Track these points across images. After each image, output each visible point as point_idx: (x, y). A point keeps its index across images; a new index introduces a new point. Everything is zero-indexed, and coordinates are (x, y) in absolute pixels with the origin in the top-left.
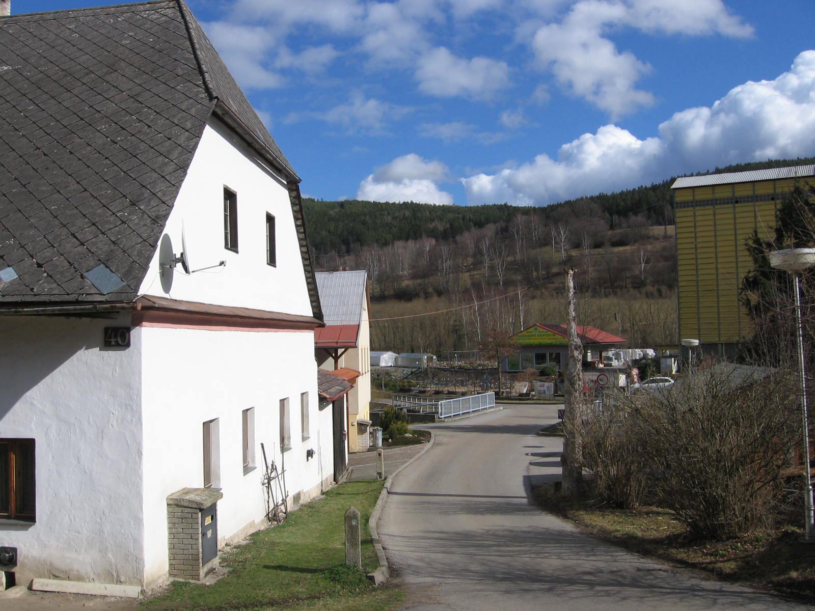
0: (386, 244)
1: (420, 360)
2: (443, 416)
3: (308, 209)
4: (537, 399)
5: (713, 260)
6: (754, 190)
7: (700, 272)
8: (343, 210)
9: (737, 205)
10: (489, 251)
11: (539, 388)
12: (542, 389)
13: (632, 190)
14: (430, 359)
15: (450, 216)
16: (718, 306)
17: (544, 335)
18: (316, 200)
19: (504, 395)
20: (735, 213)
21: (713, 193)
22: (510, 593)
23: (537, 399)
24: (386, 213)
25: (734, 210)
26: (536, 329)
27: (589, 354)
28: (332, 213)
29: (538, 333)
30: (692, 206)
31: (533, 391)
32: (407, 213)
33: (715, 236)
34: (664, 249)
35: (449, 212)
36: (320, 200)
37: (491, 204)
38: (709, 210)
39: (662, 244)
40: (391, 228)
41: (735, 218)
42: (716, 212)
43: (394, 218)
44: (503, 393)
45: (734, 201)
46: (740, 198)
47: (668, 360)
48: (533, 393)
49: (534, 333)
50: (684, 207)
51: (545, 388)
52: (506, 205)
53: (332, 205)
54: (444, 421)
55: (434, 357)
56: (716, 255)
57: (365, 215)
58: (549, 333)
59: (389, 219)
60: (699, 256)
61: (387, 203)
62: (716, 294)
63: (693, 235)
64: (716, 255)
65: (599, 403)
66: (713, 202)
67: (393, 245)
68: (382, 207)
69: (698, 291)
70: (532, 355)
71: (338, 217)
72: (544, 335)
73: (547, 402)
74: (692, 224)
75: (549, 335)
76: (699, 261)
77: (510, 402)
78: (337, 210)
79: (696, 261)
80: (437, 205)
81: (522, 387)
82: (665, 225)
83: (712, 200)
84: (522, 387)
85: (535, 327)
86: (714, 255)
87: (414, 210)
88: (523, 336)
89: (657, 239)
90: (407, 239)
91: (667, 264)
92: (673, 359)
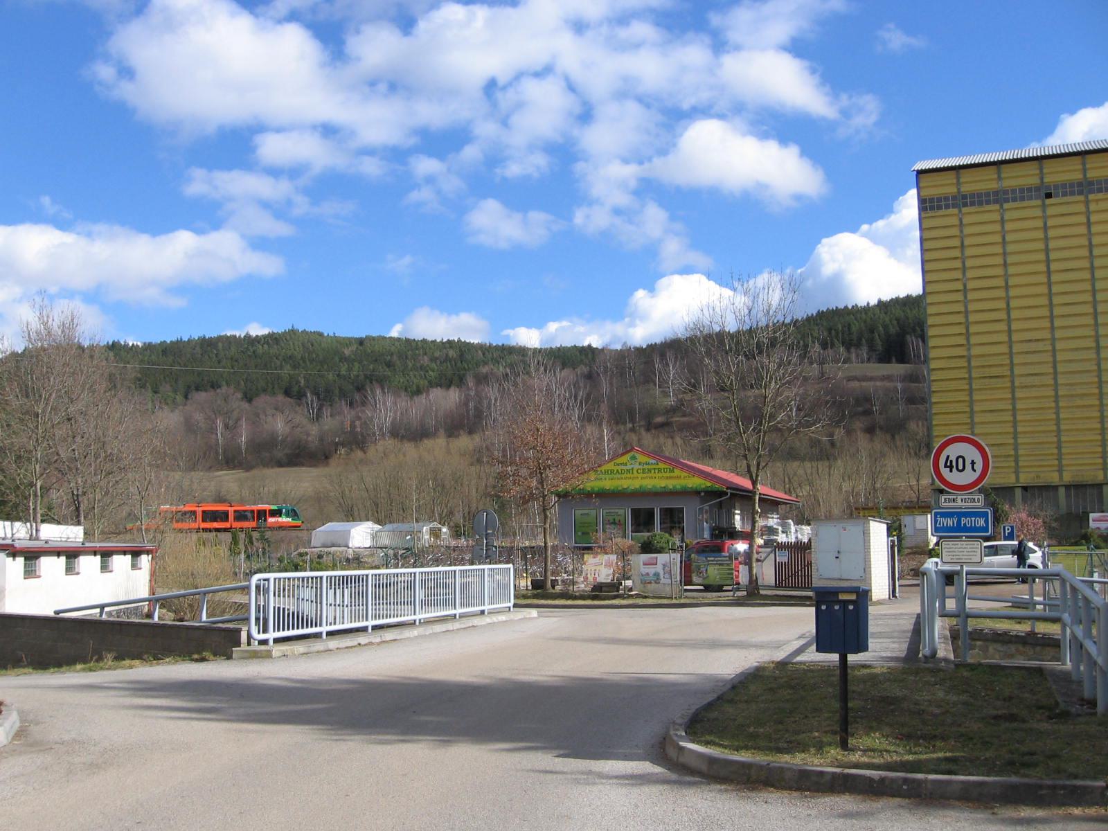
0: (418, 392)
1: (416, 534)
2: (271, 635)
3: (312, 345)
4: (638, 596)
5: (1003, 315)
6: (1085, 171)
7: (973, 340)
8: (361, 348)
9: (1048, 201)
11: (644, 570)
12: (651, 570)
14: (435, 533)
16: (1014, 410)
17: (650, 471)
18: (326, 334)
20: (1045, 218)
21: (1000, 178)
23: (638, 596)
24: (421, 353)
25: (1044, 211)
26: (634, 458)
27: (737, 518)
28: (347, 352)
29: (637, 466)
30: (954, 206)
31: (628, 579)
32: (451, 353)
33: (1005, 265)
36: (331, 334)
37: (569, 346)
38: (991, 213)
40: (427, 372)
41: (1045, 228)
42: (1006, 217)
43: (434, 359)
44: (554, 583)
45: (1043, 193)
46: (1056, 187)
48: (629, 583)
49: (629, 467)
50: (940, 208)
51: (659, 568)
52: (589, 346)
53: (349, 342)
54: (268, 655)
55: (444, 530)
56: (1008, 305)
57: (392, 355)
58: (661, 466)
59: (425, 360)
60: (971, 307)
61: (424, 341)
62: (1009, 385)
63: (958, 264)
64: (1008, 305)
66: (999, 197)
67: (428, 395)
68: (417, 345)
69: (970, 378)
71: (353, 356)
72: (650, 471)
74: (956, 242)
75: (659, 470)
76: (972, 318)
77: (570, 602)
78: (354, 347)
79: (967, 317)
80: (494, 345)
81: (599, 568)
83: (996, 193)
84: (599, 568)
86: (1002, 305)
87: (461, 350)
88: (606, 472)
90: (448, 387)
92: (929, 516)
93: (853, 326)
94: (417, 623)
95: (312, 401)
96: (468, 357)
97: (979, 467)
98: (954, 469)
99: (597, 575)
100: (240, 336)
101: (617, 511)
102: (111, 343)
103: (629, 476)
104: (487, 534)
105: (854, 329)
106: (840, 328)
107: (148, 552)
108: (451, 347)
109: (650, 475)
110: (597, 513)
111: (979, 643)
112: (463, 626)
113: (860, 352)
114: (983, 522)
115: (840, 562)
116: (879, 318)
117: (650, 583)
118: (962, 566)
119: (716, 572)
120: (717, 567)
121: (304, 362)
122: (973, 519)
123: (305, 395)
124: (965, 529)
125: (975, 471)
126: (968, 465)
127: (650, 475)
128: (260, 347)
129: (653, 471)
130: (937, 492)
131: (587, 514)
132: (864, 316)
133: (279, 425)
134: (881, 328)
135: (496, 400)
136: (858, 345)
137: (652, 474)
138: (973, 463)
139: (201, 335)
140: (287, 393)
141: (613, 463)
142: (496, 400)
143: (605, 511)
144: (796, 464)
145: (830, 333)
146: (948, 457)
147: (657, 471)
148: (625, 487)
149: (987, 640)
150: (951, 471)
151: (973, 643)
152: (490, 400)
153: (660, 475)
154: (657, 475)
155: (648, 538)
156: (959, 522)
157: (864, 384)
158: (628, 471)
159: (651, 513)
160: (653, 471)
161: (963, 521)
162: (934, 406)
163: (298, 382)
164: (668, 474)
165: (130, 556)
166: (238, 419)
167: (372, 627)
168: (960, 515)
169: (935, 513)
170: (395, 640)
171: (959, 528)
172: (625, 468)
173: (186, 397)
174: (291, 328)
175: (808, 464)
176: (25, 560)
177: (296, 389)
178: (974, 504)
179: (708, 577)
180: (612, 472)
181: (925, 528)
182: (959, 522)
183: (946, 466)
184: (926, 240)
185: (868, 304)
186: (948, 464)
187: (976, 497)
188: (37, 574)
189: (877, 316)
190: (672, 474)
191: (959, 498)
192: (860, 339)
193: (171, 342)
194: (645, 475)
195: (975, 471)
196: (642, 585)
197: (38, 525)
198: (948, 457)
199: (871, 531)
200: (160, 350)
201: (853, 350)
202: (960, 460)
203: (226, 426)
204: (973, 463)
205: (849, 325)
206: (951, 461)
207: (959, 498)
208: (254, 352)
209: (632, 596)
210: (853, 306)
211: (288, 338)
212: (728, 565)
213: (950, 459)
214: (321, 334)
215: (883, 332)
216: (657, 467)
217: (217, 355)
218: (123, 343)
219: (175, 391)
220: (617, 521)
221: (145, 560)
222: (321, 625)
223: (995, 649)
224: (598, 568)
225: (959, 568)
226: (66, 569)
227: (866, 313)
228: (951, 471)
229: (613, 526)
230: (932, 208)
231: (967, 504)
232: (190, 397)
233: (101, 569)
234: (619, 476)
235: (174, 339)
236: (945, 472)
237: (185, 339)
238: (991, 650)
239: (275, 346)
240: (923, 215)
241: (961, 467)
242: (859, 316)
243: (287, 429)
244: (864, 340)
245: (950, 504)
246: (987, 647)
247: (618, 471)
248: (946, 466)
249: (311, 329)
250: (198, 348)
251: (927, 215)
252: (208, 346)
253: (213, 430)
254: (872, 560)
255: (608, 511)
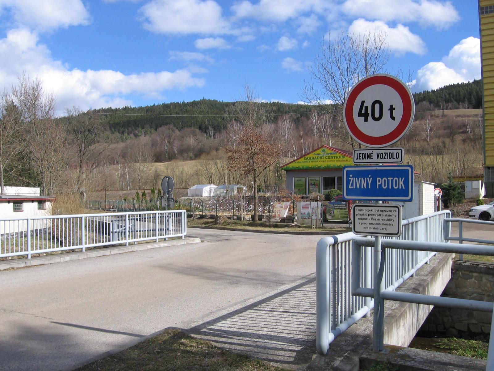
4: (296, 226)
10: (317, 122)
11: (303, 211)
13: (419, 93)
15: (302, 110)
17: (332, 157)
19: (264, 219)
22: (458, 115)
26: (324, 151)
29: (325, 156)
32: (274, 108)
34: (443, 123)
35: (301, 108)
36: (221, 101)
39: (441, 120)
47: (475, 183)
49: (321, 155)
55: (244, 188)
58: (338, 155)
65: (358, 246)
70: (320, 179)
72: (332, 157)
73: (306, 230)
75: (337, 157)
82: (443, 109)
84: (282, 210)
85: (323, 149)
88: (310, 158)
89: (438, 117)
91: (444, 131)
92: (480, 181)
93: (461, 92)
94: (127, 244)
95: (211, 131)
96: (282, 110)
97: (399, 114)
98: (370, 118)
99: (280, 214)
100: (180, 103)
101: (315, 178)
102: (124, 107)
103: (321, 160)
104: (169, 191)
105: (461, 93)
106: (455, 93)
107: (51, 201)
108: (274, 106)
109: (332, 160)
110: (305, 179)
111: (475, 274)
112: (121, 252)
113: (464, 105)
114: (401, 183)
115: (405, 209)
116: (474, 88)
117: (306, 218)
118: (376, 237)
119: (339, 213)
120: (339, 210)
121: (208, 114)
122: (390, 179)
123: (208, 128)
124: (381, 192)
125: (393, 118)
126: (386, 113)
127: (332, 160)
128: (189, 107)
129: (333, 158)
130: (487, 169)
131: (300, 180)
132: (466, 87)
133: (191, 142)
134: (475, 93)
135: (288, 128)
136: (463, 101)
137: (333, 159)
138: (392, 109)
139: (163, 102)
140: (200, 128)
141: (313, 153)
142: (288, 128)
143: (309, 178)
144: (425, 157)
145: (450, 95)
146: (363, 102)
147: (335, 157)
148: (319, 166)
149: (481, 273)
150: (366, 120)
151: (470, 274)
152: (286, 128)
153: (337, 159)
154: (336, 159)
155: (329, 192)
156: (374, 183)
157: (464, 119)
158: (321, 157)
159: (333, 180)
160: (333, 158)
161: (379, 181)
162: (486, 122)
163: (205, 123)
164: (341, 159)
165: (36, 203)
166: (174, 139)
167: (184, 236)
168: (376, 174)
169: (347, 171)
170: (43, 264)
171: (373, 191)
172: (319, 156)
173: (156, 130)
174: (203, 98)
175: (432, 157)
176: (14, 204)
177: (204, 126)
178: (392, 160)
179: (334, 216)
180: (313, 158)
181: (478, 188)
182: (374, 183)
183: (360, 115)
184: (483, 30)
185: (469, 82)
186: (363, 112)
187: (395, 152)
188: (22, 210)
189: (473, 88)
190: (343, 159)
191: (375, 152)
192: (464, 98)
193: (151, 106)
194: (329, 160)
195: (393, 118)
196: (302, 220)
197: (3, 187)
198: (363, 102)
199: (423, 190)
200: (145, 110)
201: (461, 103)
202: (377, 106)
203: (169, 142)
204: (392, 109)
205: (459, 92)
206: (366, 108)
207: (375, 152)
208: (186, 110)
209: (293, 226)
210: (461, 83)
211: (201, 103)
212: (345, 209)
213: (365, 105)
214: (216, 101)
215: (475, 95)
216: (335, 155)
217: (170, 112)
218: (129, 107)
219: (151, 128)
220: (315, 184)
221: (48, 205)
222: (155, 236)
223: (487, 279)
224: (280, 209)
225: (373, 239)
226: (14, 209)
227: (467, 87)
228: (366, 120)
229: (314, 186)
230: (487, 12)
231: (383, 160)
232: (157, 130)
233: (14, 210)
234: (316, 160)
235: (152, 105)
236: (359, 121)
237: (156, 105)
238: (484, 279)
239: (195, 107)
240: (482, 16)
241: (377, 115)
242: (464, 88)
243: (196, 144)
244: (466, 98)
245: (365, 161)
246: (481, 278)
247: (316, 158)
248: (360, 115)
249: (211, 99)
250: (162, 109)
251: (483, 16)
252: (166, 107)
253: (163, 144)
254: (424, 208)
255: (311, 178)
